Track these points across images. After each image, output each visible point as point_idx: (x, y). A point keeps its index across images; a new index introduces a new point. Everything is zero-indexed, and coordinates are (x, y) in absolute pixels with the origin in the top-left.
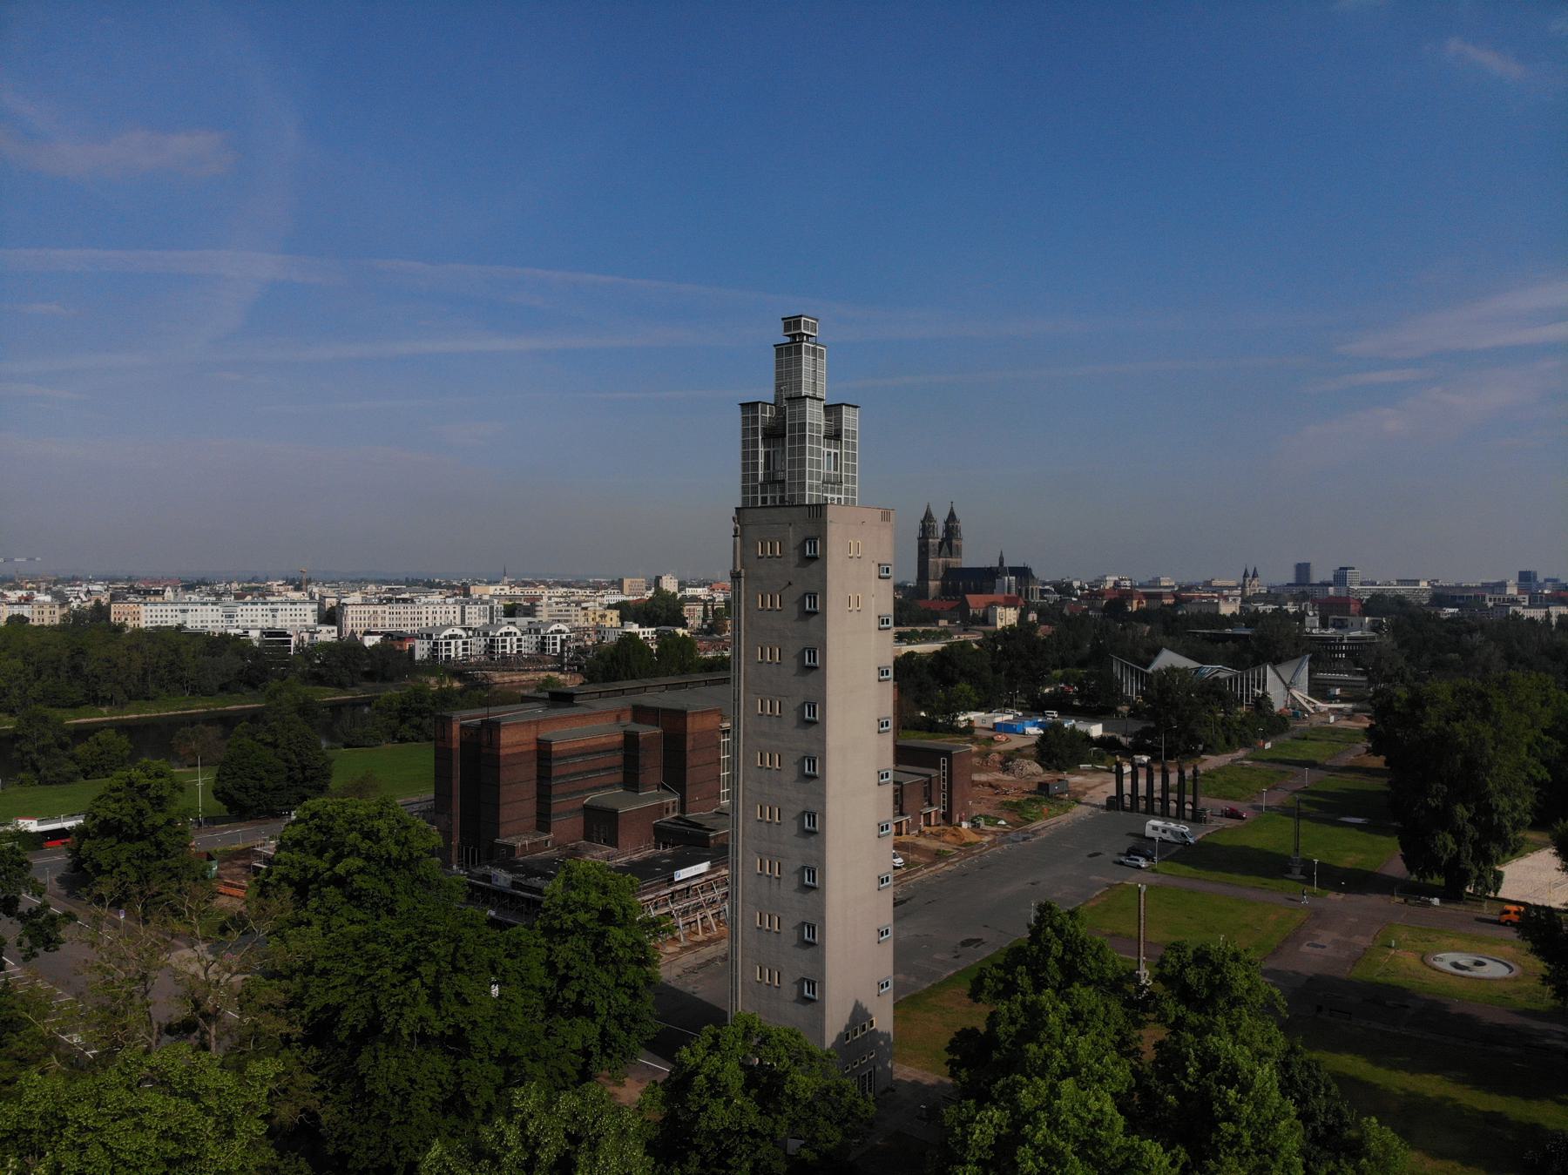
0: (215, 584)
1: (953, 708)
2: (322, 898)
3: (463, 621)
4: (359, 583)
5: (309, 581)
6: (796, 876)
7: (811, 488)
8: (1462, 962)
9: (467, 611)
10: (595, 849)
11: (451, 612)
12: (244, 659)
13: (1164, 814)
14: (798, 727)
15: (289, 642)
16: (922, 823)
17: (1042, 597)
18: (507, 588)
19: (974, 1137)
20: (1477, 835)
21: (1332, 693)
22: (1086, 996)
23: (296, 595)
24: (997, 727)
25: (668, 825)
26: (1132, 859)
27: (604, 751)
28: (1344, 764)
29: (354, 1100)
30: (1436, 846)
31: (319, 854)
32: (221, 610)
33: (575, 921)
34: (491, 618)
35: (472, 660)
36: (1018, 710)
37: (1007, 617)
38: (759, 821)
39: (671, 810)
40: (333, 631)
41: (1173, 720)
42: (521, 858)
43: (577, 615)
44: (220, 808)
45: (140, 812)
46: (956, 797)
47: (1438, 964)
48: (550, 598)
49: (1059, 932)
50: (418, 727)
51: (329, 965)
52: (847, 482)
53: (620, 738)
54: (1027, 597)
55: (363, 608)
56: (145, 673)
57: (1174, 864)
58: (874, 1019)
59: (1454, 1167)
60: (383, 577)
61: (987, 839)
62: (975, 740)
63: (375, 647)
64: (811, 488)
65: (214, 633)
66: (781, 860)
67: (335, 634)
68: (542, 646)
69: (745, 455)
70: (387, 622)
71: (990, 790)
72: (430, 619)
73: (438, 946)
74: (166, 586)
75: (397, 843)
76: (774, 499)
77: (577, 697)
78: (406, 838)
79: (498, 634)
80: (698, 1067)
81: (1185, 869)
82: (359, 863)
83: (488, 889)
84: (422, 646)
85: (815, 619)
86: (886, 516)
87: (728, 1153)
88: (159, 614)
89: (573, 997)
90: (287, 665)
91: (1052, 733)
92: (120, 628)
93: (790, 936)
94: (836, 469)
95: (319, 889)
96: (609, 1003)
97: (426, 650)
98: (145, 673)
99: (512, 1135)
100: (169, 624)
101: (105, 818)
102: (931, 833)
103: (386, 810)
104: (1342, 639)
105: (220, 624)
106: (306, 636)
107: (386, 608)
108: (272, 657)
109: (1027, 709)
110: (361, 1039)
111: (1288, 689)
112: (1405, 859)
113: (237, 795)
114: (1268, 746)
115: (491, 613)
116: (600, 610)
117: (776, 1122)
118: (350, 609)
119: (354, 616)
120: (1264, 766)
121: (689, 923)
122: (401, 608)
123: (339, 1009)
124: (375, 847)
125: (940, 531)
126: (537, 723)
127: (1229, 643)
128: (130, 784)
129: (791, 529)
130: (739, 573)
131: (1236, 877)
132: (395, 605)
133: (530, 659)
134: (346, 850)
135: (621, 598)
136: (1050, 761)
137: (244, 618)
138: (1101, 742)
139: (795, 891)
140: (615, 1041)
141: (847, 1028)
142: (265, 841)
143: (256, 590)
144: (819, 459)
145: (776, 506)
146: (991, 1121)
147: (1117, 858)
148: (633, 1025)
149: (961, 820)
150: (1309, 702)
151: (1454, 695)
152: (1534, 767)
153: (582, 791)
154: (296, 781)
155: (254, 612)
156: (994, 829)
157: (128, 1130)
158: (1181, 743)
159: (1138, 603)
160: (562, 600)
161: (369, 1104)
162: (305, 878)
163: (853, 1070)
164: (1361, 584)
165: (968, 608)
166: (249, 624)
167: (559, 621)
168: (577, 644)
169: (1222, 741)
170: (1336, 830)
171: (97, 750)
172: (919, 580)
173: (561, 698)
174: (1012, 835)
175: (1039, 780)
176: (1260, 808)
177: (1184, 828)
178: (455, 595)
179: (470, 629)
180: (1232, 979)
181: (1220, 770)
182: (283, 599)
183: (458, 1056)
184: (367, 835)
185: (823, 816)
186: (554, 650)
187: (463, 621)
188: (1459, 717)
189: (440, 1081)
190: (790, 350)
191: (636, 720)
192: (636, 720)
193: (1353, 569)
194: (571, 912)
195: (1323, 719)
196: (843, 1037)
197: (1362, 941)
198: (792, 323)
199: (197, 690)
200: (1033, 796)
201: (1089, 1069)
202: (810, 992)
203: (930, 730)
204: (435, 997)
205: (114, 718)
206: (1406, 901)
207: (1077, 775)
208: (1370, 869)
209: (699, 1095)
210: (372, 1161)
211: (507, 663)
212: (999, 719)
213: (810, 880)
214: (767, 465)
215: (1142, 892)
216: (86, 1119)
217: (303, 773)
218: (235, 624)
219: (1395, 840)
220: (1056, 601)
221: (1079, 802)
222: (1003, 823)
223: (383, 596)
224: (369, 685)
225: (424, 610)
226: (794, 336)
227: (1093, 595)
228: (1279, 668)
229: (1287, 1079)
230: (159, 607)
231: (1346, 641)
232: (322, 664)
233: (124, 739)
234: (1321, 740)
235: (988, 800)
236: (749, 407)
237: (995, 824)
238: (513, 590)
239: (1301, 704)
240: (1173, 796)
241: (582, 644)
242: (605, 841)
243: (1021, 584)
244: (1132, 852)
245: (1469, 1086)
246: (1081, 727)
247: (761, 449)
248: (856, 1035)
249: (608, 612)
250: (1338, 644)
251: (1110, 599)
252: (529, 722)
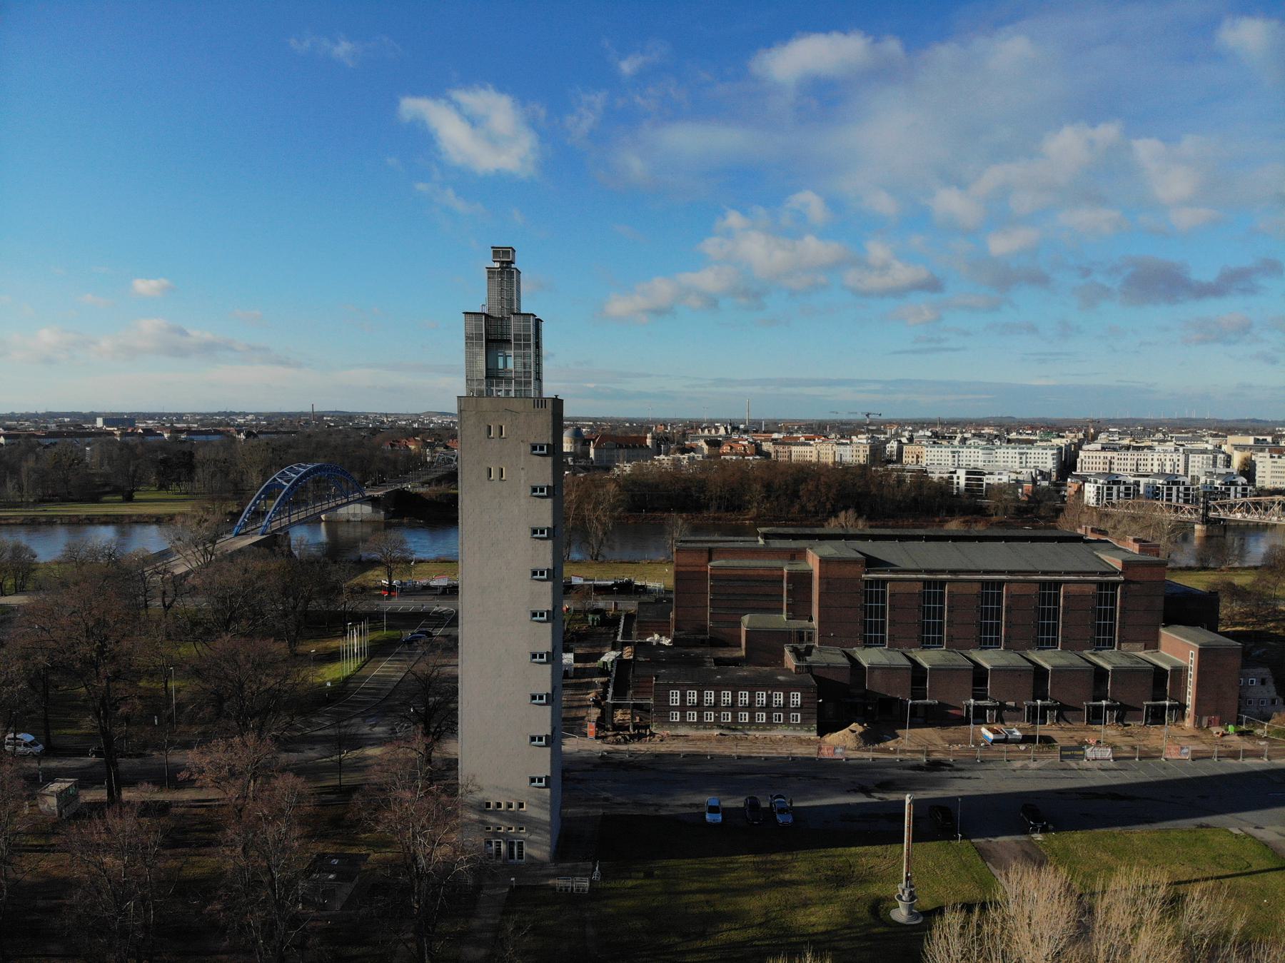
9: (1191, 459)
63: (1043, 488)
152: (597, 536)
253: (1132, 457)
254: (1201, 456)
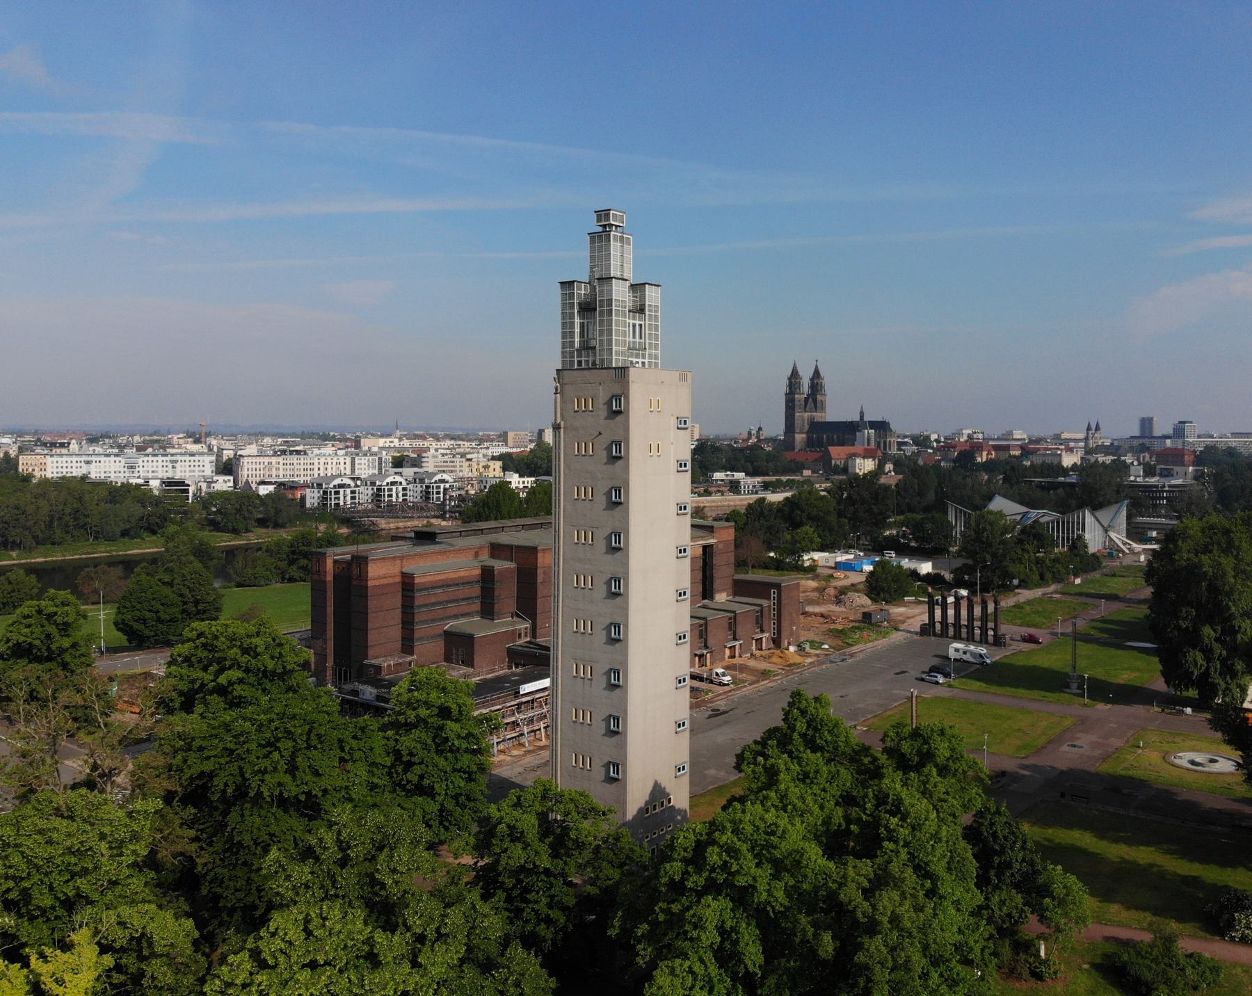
0: (117, 436)
1: (797, 549)
2: (207, 705)
3: (353, 471)
4: (256, 435)
5: (208, 434)
6: (605, 677)
7: (618, 354)
8: (1198, 760)
9: (357, 462)
10: (453, 669)
11: (342, 463)
12: (144, 507)
13: (970, 639)
14: (607, 553)
15: (187, 491)
16: (754, 647)
17: (899, 449)
18: (396, 441)
19: (679, 841)
20: (1224, 653)
21: (1149, 535)
22: (814, 759)
23: (195, 448)
24: (838, 566)
25: (520, 648)
26: (931, 676)
27: (463, 584)
28: (1142, 597)
29: (225, 851)
30: (1187, 661)
31: (205, 669)
32: (123, 461)
33: (417, 716)
34: (380, 469)
35: (360, 508)
36: (860, 551)
37: (865, 466)
38: (575, 632)
39: (523, 635)
40: (229, 480)
41: (988, 557)
42: (387, 677)
43: (461, 466)
44: (120, 638)
45: (48, 636)
46: (785, 624)
47: (1177, 761)
48: (436, 450)
49: (803, 712)
50: (304, 568)
51: (204, 743)
52: (650, 348)
53: (479, 572)
54: (885, 449)
55: (258, 460)
56: (51, 521)
57: (969, 681)
58: (671, 797)
59: (1145, 917)
60: (276, 431)
61: (809, 660)
62: (816, 577)
64: (618, 354)
65: (117, 483)
66: (592, 664)
67: (231, 484)
68: (427, 495)
69: (564, 325)
70: (281, 473)
71: (822, 620)
72: (322, 469)
73: (295, 726)
74: (71, 439)
75: (272, 658)
76: (587, 362)
77: (439, 536)
78: (280, 653)
79: (385, 483)
80: (502, 818)
81: (977, 685)
82: (240, 674)
83: (356, 702)
84: (313, 495)
85: (620, 462)
86: (683, 378)
87: (527, 890)
88: (65, 465)
89: (415, 779)
90: (185, 513)
91: (879, 569)
92: (27, 479)
93: (600, 728)
94: (641, 338)
95: (204, 697)
96: (447, 785)
97: (316, 498)
98: (51, 521)
99: (329, 838)
100: (74, 475)
101: (18, 641)
102: (762, 656)
103: (263, 629)
104: (1163, 486)
105: (122, 475)
106: (204, 486)
107: (280, 459)
108: (171, 505)
109: (869, 550)
110: (228, 803)
111: (1106, 531)
112: (1164, 673)
113: (136, 626)
114: (1078, 581)
115: (380, 464)
116: (483, 462)
117: (565, 863)
118: (245, 460)
119: (250, 467)
120: (1069, 599)
121: (534, 731)
122: (294, 459)
123: (211, 775)
124: (253, 661)
125: (806, 388)
126: (402, 558)
127: (1060, 491)
128: (40, 612)
129: (601, 388)
130: (559, 424)
131: (1021, 692)
132: (289, 457)
133: (415, 507)
134: (228, 663)
135: (504, 450)
136: (878, 594)
137: (145, 469)
138: (928, 578)
139: (605, 689)
140: (451, 815)
141: (647, 803)
142: (156, 664)
143: (157, 443)
144: (622, 329)
145: (589, 369)
146: (694, 830)
147: (919, 676)
148: (467, 803)
149: (789, 644)
150: (1125, 544)
151: (1203, 531)
153: (443, 619)
154: (190, 614)
155: (155, 464)
156: (817, 652)
157: (41, 843)
158: (996, 579)
159: (987, 454)
160: (448, 451)
161: (237, 853)
162: (193, 689)
163: (652, 839)
164: (1199, 437)
165: (831, 459)
166: (150, 475)
167: (444, 471)
168: (459, 492)
169: (1036, 577)
170: (1119, 652)
171: (9, 588)
172: (786, 433)
173: (425, 537)
174: (832, 658)
175: (865, 610)
176: (1056, 634)
177: (983, 650)
178: (347, 447)
179: (358, 479)
180: (936, 748)
181: (1029, 602)
182: (183, 451)
183: (311, 818)
184: (246, 651)
185: (626, 626)
186: (438, 499)
187: (353, 471)
188: (1206, 550)
189: (295, 837)
190: (600, 238)
191: (492, 556)
192: (492, 556)
193: (1191, 422)
194: (414, 709)
195: (1135, 558)
196: (643, 811)
197: (1115, 742)
198: (603, 215)
199: (99, 535)
200: (857, 624)
201: (794, 806)
202: (614, 773)
203: (777, 569)
204: (292, 769)
205: (23, 561)
206: (1163, 710)
207: (901, 606)
208: (1140, 685)
209: (501, 841)
210: (239, 900)
211: (392, 510)
212: (842, 557)
213: (615, 681)
214: (582, 334)
215: (914, 696)
216: (8, 838)
217: (196, 607)
218: (137, 475)
219: (1157, 659)
220: (913, 452)
221: (897, 629)
222: (826, 647)
223: (277, 448)
224: (263, 530)
225: (316, 461)
226: (604, 226)
227: (948, 446)
228: (1098, 514)
229: (991, 834)
230: (65, 459)
231: (1167, 489)
232: (219, 511)
233: (33, 578)
234: (1128, 577)
235: (817, 628)
236: (567, 285)
237: (819, 648)
238: (402, 443)
239: (1118, 546)
240: (977, 623)
241: (463, 492)
242: (463, 662)
243: (880, 437)
244: (934, 669)
245: (1176, 857)
246: (906, 563)
247: (577, 321)
248: (655, 809)
249: (491, 463)
250: (1159, 492)
251: (961, 451)
252: (394, 557)
253: (299, 461)
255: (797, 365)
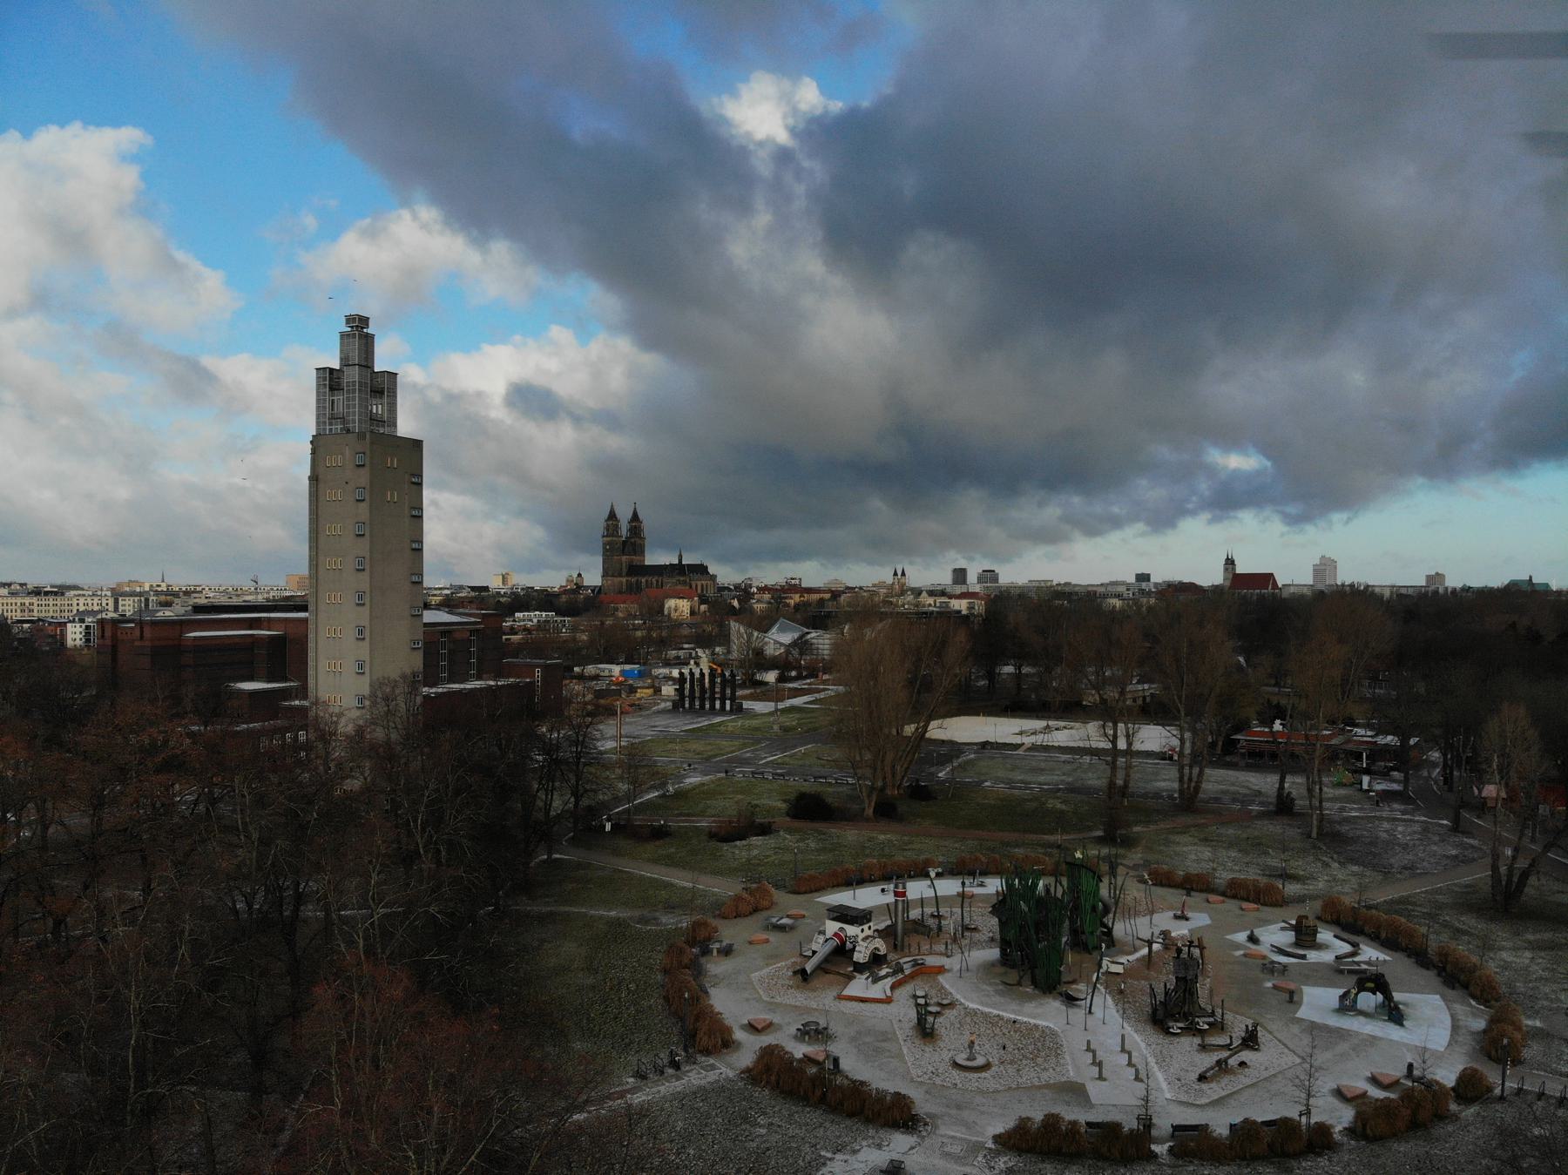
9: (121, 603)
129: (347, 448)
225: (75, 602)
254: (132, 599)
255: (615, 508)
